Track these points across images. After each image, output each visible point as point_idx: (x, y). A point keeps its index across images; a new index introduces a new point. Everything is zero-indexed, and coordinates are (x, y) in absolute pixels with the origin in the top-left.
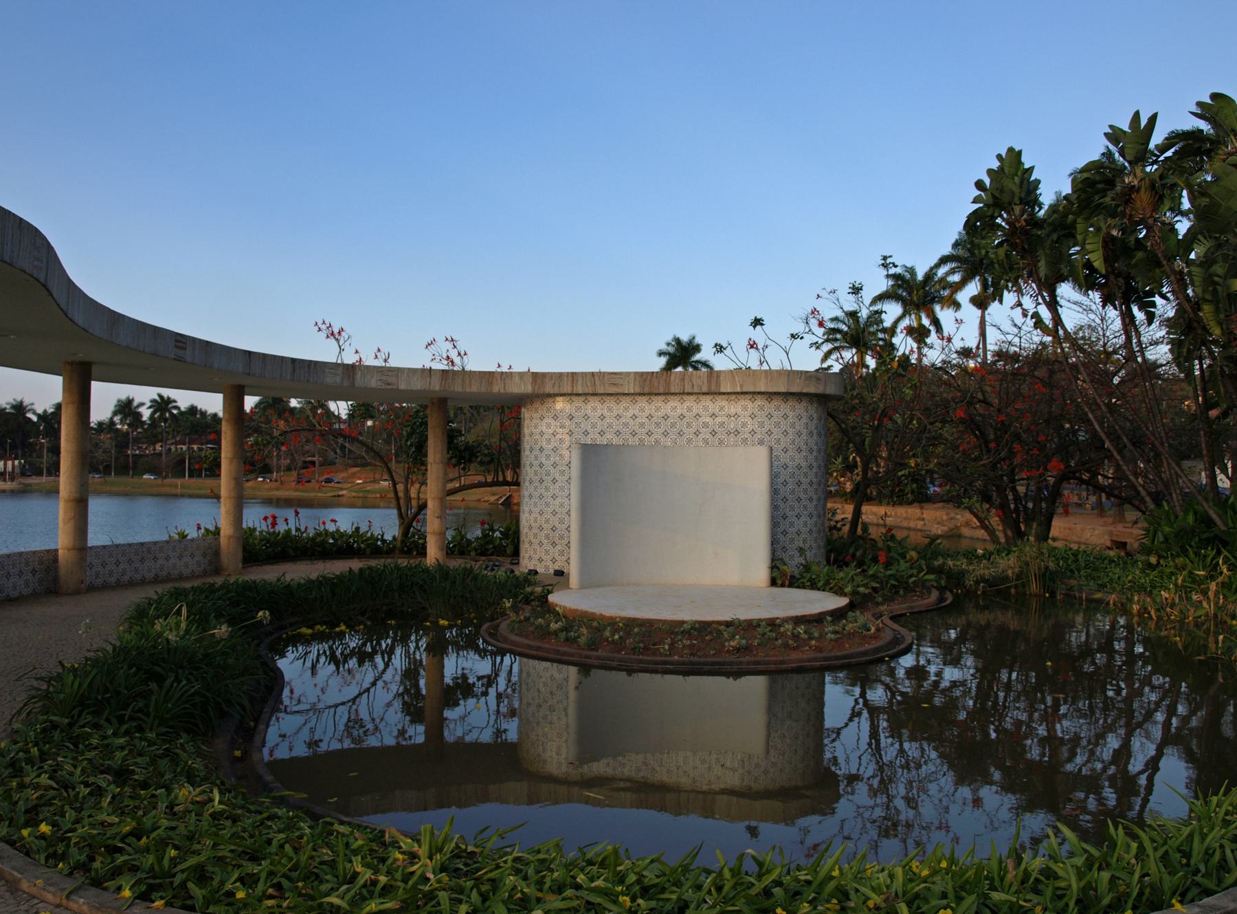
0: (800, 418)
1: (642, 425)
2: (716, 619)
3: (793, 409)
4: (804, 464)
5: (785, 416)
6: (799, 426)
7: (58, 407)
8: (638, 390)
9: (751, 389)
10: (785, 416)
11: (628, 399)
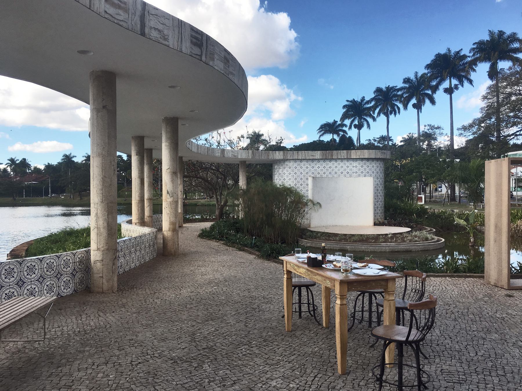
0: (378, 167)
1: (322, 170)
2: (358, 233)
3: (376, 164)
4: (379, 183)
5: (373, 167)
6: (378, 170)
7: (88, 158)
8: (321, 158)
9: (363, 157)
10: (373, 167)
11: (317, 161)
